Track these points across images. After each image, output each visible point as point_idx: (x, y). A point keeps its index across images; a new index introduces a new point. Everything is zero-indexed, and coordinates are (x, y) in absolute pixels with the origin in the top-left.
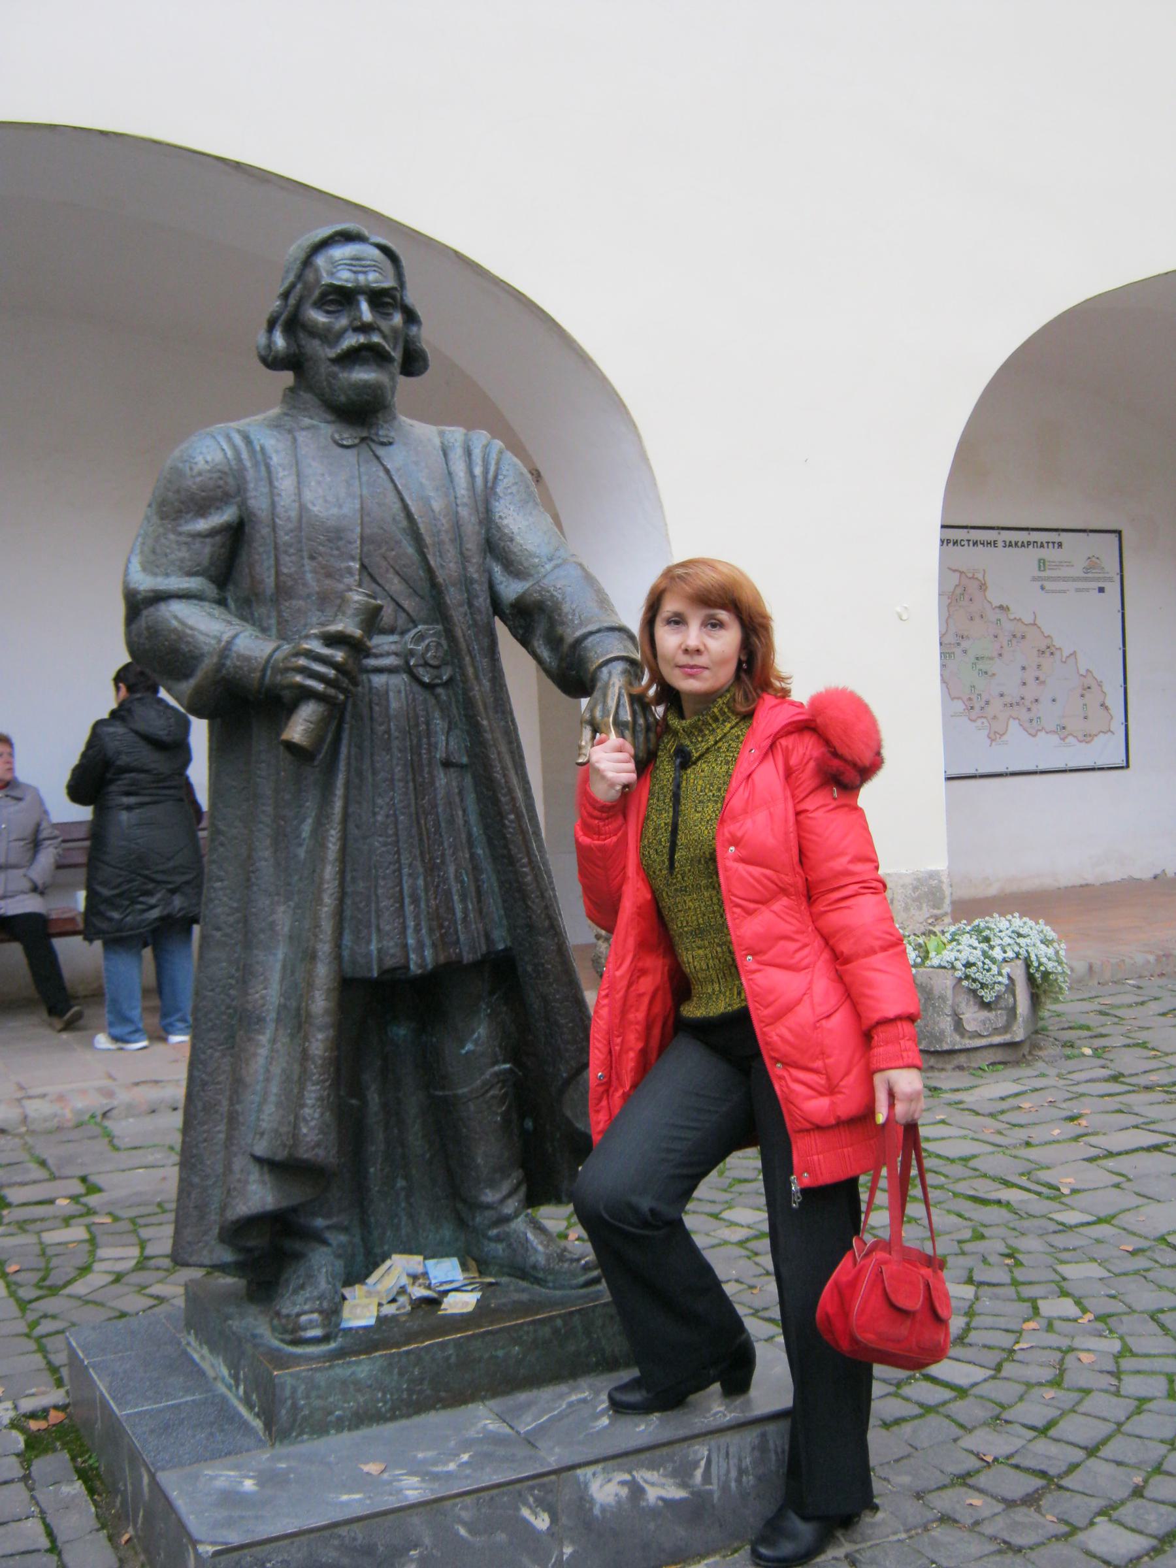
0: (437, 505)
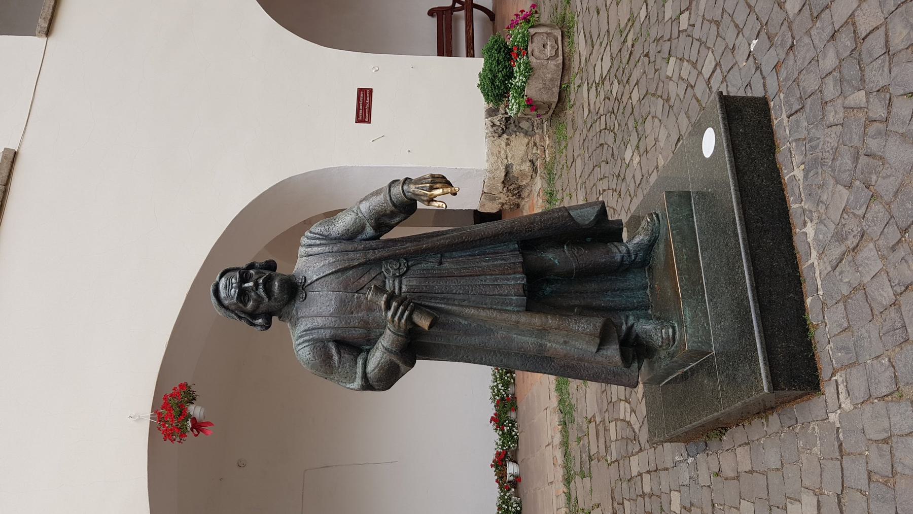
0: (331, 260)
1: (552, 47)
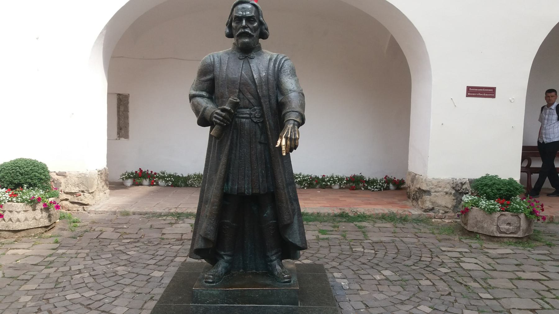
1: (508, 230)
